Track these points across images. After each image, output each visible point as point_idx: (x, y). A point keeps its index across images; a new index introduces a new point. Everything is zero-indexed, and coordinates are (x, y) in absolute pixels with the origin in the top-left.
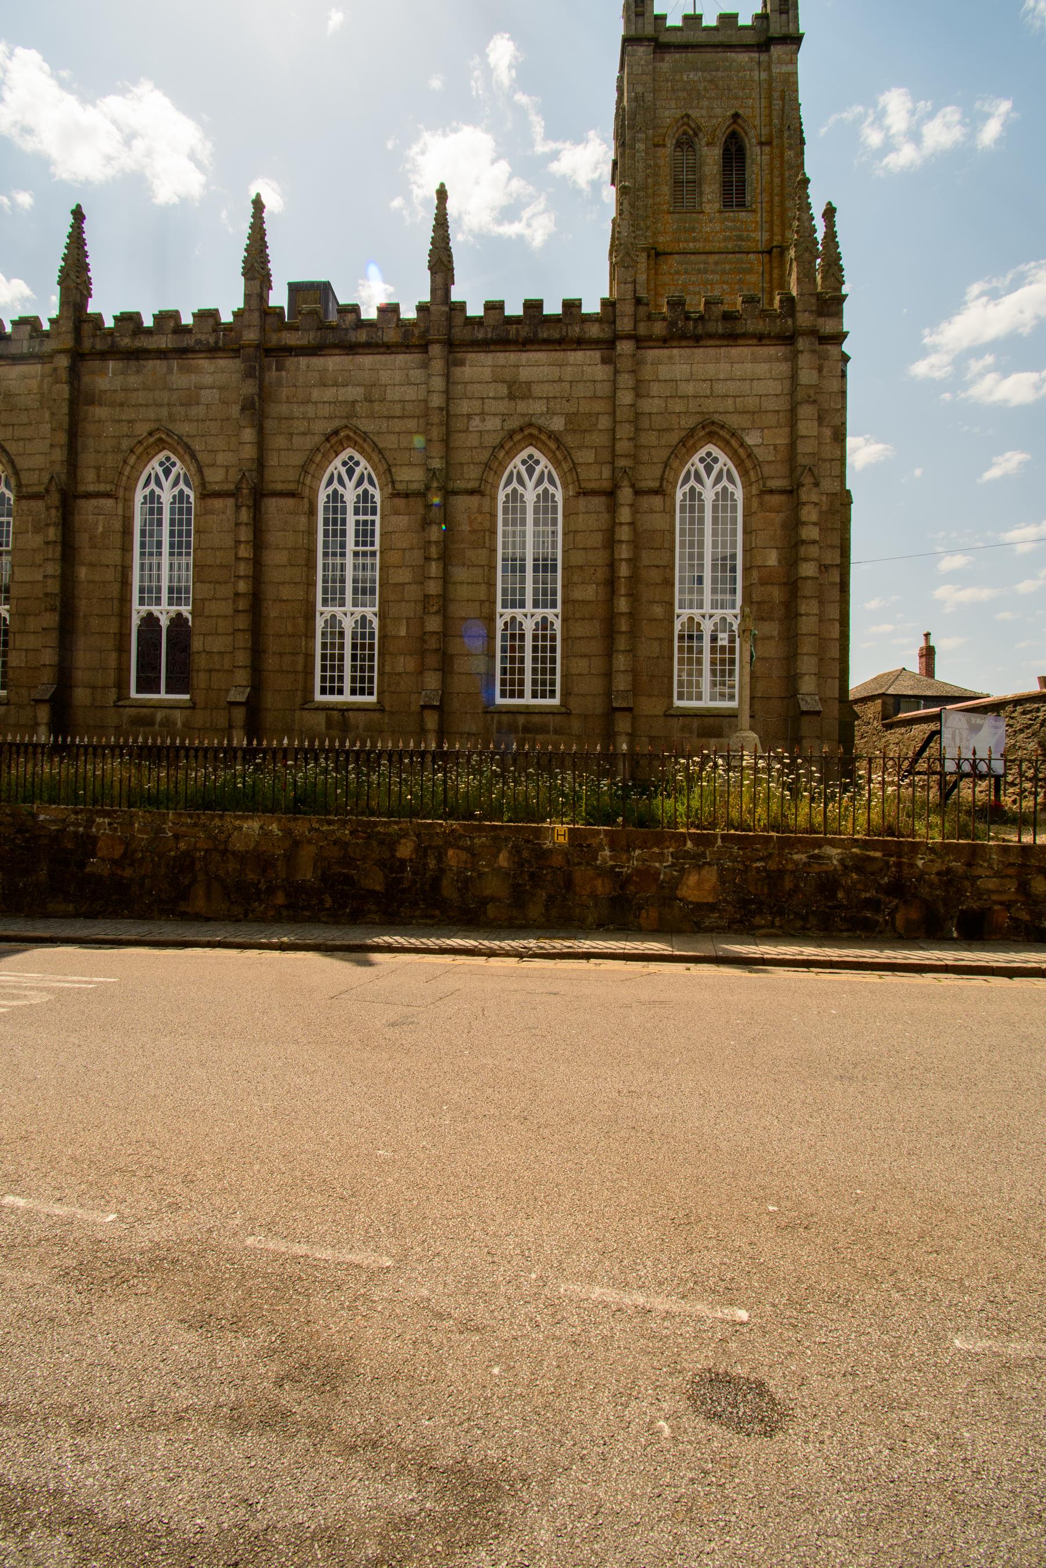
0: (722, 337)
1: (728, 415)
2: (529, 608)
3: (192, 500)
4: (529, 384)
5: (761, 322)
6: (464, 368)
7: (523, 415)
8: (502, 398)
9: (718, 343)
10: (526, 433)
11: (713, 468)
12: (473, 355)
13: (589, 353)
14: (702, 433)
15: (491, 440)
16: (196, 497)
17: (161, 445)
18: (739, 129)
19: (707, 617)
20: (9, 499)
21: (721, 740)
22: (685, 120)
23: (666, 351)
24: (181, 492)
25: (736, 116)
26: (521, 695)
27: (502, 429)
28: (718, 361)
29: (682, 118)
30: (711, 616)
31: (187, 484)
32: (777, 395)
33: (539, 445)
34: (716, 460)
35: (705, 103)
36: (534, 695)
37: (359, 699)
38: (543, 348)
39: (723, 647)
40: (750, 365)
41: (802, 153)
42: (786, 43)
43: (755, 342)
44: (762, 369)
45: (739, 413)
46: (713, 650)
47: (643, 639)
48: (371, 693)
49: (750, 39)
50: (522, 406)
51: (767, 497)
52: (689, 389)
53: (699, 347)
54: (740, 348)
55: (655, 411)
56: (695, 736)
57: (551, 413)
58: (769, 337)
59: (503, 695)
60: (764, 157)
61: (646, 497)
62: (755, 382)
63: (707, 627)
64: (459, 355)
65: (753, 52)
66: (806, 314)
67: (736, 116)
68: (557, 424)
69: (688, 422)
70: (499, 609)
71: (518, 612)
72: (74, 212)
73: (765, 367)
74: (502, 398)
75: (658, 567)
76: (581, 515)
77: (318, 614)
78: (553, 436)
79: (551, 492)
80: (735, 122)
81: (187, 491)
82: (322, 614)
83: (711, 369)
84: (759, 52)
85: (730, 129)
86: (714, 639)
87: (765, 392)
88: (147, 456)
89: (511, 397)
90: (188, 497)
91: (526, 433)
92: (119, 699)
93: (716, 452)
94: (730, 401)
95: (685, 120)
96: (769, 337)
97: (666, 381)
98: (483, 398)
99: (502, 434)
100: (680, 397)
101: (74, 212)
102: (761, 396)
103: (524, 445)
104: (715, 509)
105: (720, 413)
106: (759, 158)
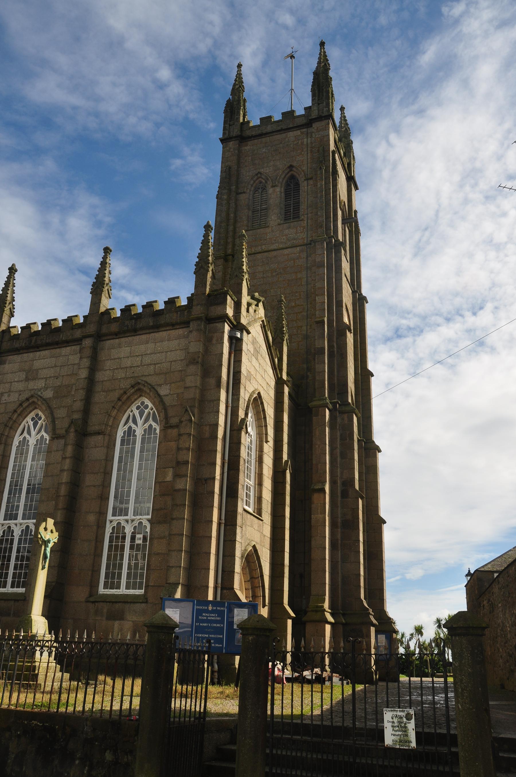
0: (152, 327)
1: (150, 377)
2: (20, 520)
3: (158, 431)
4: (37, 370)
5: (175, 314)
6: (5, 365)
7: (31, 390)
8: (22, 381)
9: (148, 331)
10: (30, 401)
11: (38, 423)
12: (11, 357)
13: (73, 347)
14: (133, 391)
15: (12, 407)
16: (160, 430)
17: (34, 406)
18: (295, 174)
19: (130, 522)
20: (46, 439)
21: (122, 622)
22: (259, 175)
23: (117, 340)
24: (151, 426)
25: (291, 167)
26: (118, 587)
27: (18, 400)
28: (147, 342)
29: (257, 175)
30: (133, 521)
31: (155, 420)
32: (182, 360)
33: (146, 395)
34: (147, 407)
35: (272, 163)
36: (127, 588)
37: (15, 590)
38: (48, 348)
39: (138, 545)
40: (166, 342)
41: (216, 209)
42: (322, 120)
43: (171, 327)
44: (174, 344)
45: (157, 374)
46: (132, 547)
47: (79, 540)
48: (140, 588)
49: (304, 121)
50: (31, 385)
51: (169, 431)
52: (128, 363)
53: (137, 335)
54: (161, 333)
55: (106, 379)
56: (104, 618)
57: (46, 388)
58: (177, 324)
59: (105, 587)
60: (309, 187)
61: (93, 437)
62: (169, 353)
63: (129, 530)
64: (4, 358)
65: (304, 128)
66: (199, 307)
67: (291, 167)
68: (49, 394)
69: (125, 384)
70: (110, 517)
71: (121, 518)
72: (9, 269)
73: (176, 342)
74: (22, 381)
75: (94, 486)
76: (53, 452)
77: (108, 523)
78: (45, 401)
79: (154, 427)
80: (291, 170)
81: (154, 425)
82: (111, 522)
83: (142, 348)
84: (307, 128)
85: (289, 174)
86: (133, 538)
87: (174, 359)
88: (23, 415)
89: (27, 379)
90: (155, 429)
91: (30, 401)
92: (91, 595)
93: (147, 402)
94: (152, 367)
95: (259, 175)
96: (177, 324)
97: (114, 359)
98: (11, 382)
99: (18, 403)
100: (122, 368)
101: (9, 269)
102: (171, 362)
103: (31, 409)
104: (143, 440)
105: (145, 376)
106: (306, 188)
